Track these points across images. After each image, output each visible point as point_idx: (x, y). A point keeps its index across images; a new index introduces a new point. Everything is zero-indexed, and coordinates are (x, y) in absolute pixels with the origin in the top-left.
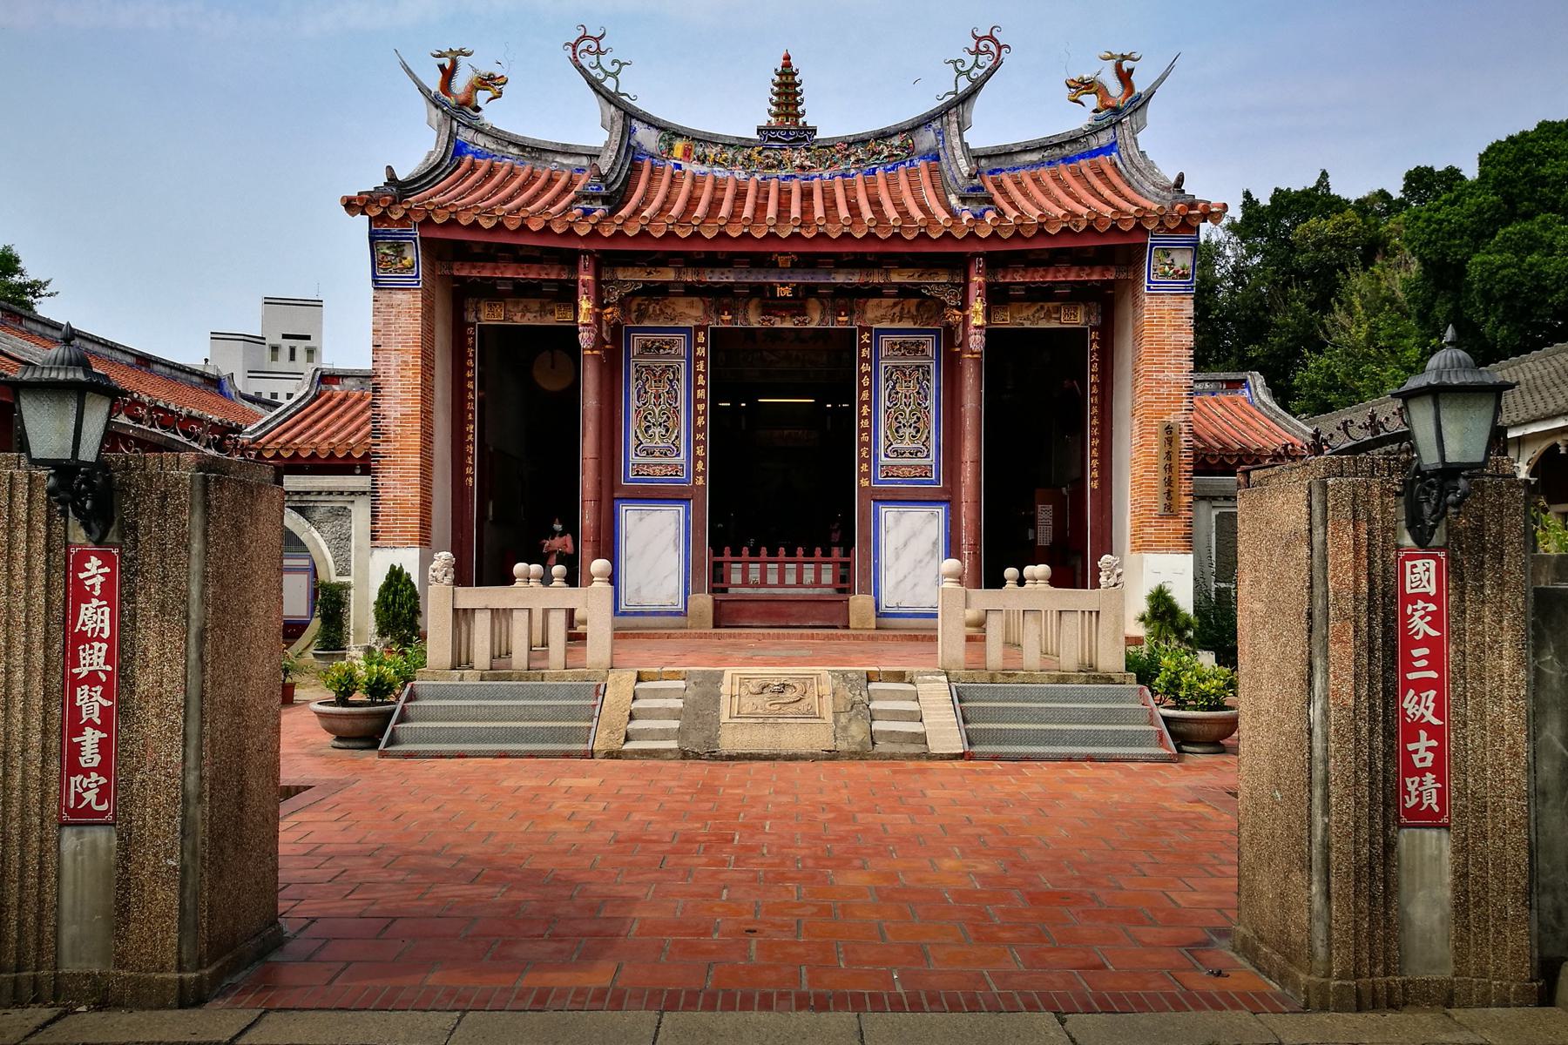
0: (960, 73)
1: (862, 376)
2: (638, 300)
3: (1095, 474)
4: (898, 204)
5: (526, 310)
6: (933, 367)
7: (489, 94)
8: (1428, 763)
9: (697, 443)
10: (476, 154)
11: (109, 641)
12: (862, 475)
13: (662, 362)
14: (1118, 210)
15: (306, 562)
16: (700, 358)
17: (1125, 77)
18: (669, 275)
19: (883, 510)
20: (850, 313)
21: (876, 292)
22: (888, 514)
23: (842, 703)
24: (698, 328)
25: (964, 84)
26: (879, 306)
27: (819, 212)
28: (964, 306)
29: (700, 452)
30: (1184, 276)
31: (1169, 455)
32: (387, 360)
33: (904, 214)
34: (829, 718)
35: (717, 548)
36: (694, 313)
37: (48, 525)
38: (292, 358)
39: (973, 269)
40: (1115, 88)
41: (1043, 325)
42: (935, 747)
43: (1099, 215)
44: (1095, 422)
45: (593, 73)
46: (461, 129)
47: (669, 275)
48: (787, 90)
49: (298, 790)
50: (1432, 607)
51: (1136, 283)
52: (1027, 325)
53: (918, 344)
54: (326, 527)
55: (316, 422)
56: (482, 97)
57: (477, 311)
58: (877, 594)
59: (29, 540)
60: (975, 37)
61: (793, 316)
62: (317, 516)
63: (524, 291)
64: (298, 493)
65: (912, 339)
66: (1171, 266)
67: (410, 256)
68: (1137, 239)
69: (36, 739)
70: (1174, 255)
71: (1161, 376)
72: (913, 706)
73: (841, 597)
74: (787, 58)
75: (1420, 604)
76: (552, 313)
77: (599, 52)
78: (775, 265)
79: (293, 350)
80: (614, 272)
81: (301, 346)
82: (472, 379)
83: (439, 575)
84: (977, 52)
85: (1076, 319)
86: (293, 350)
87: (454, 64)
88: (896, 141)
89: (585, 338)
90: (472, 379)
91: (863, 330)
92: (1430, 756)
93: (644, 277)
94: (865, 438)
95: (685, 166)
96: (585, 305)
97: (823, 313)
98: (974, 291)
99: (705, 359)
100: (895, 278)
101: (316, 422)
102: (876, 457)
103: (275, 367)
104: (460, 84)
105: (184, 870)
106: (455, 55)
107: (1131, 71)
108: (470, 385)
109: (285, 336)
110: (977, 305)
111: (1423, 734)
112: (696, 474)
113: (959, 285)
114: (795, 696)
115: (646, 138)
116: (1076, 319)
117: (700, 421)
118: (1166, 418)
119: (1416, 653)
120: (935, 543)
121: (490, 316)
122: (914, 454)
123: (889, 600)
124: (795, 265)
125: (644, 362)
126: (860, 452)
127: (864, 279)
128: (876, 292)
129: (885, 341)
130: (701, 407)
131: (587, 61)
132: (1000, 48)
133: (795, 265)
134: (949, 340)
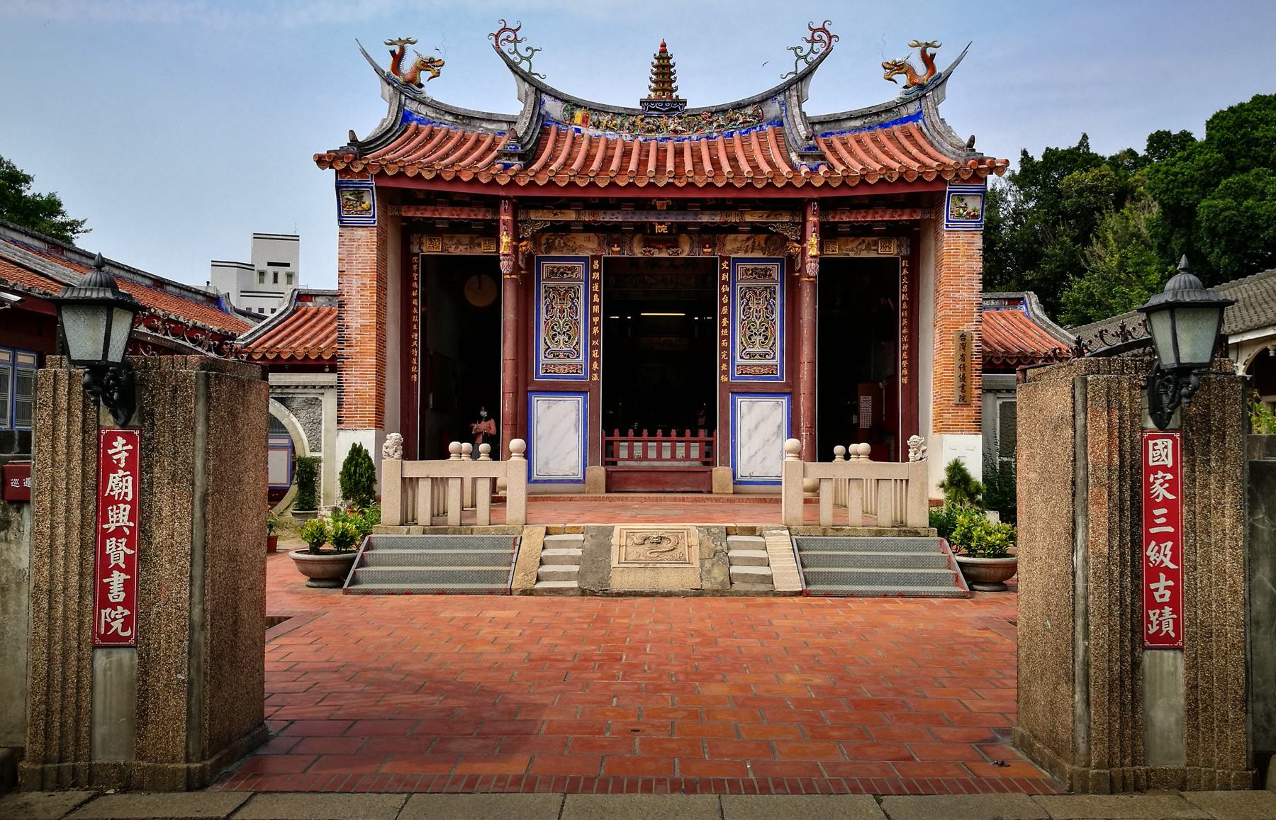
0: (800, 57)
1: (722, 295)
2: (547, 236)
3: (905, 372)
4: (750, 160)
5: (459, 243)
6: (778, 288)
7: (430, 74)
8: (1166, 599)
9: (593, 348)
10: (419, 121)
11: (132, 503)
12: (723, 373)
13: (566, 284)
14: (923, 165)
15: (286, 441)
16: (595, 281)
17: (928, 61)
18: (571, 216)
19: (739, 400)
20: (713, 245)
21: (733, 229)
22: (743, 403)
23: (706, 551)
24: (594, 258)
25: (802, 66)
26: (735, 240)
27: (688, 166)
28: (802, 240)
29: (595, 355)
30: (975, 216)
31: (963, 357)
32: (350, 282)
33: (756, 168)
34: (697, 564)
35: (608, 430)
36: (591, 245)
37: (84, 412)
38: (276, 281)
39: (810, 212)
40: (920, 69)
41: (864, 255)
42: (780, 586)
43: (908, 169)
44: (905, 331)
45: (512, 57)
46: (408, 101)
47: (571, 216)
48: (664, 71)
49: (280, 620)
50: (1169, 477)
51: (937, 222)
52: (852, 255)
53: (766, 270)
54: (302, 414)
55: (294, 331)
56: (424, 76)
57: (421, 244)
58: (734, 466)
59: (69, 424)
60: (811, 29)
61: (668, 248)
62: (295, 405)
63: (457, 228)
64: (280, 387)
65: (761, 266)
66: (965, 208)
67: (368, 201)
68: (938, 188)
69: (74, 580)
70: (967, 200)
71: (957, 295)
72: (762, 554)
73: (706, 468)
74: (664, 45)
75: (1160, 474)
76: (479, 245)
77: (516, 41)
78: (654, 208)
79: (276, 275)
80: (527, 214)
81: (282, 271)
82: (417, 297)
83: (391, 451)
84: (813, 41)
85: (890, 250)
86: (276, 275)
87: (403, 50)
88: (749, 111)
89: (505, 266)
90: (417, 297)
91: (723, 259)
92: (1168, 593)
93: (552, 218)
94: (724, 343)
95: (583, 130)
96: (505, 239)
97: (692, 246)
98: (810, 228)
99: (599, 281)
100: (748, 218)
101: (294, 331)
102: (733, 358)
103: (262, 288)
104: (407, 66)
105: (190, 682)
106: (403, 43)
107: (933, 56)
108: (415, 302)
109: (269, 264)
110: (813, 240)
111: (1162, 576)
112: (592, 372)
113: (798, 224)
114: (669, 546)
115: (553, 108)
116: (890, 250)
117: (596, 330)
118: (961, 328)
119: (1157, 512)
120: (780, 427)
121: (430, 248)
122: (763, 356)
123: (743, 470)
124: (670, 208)
125: (551, 284)
126: (721, 355)
127: (724, 219)
128: (733, 229)
129: (740, 267)
130: (596, 319)
131: (507, 48)
132: (830, 38)
133: (670, 208)
134: (791, 267)
